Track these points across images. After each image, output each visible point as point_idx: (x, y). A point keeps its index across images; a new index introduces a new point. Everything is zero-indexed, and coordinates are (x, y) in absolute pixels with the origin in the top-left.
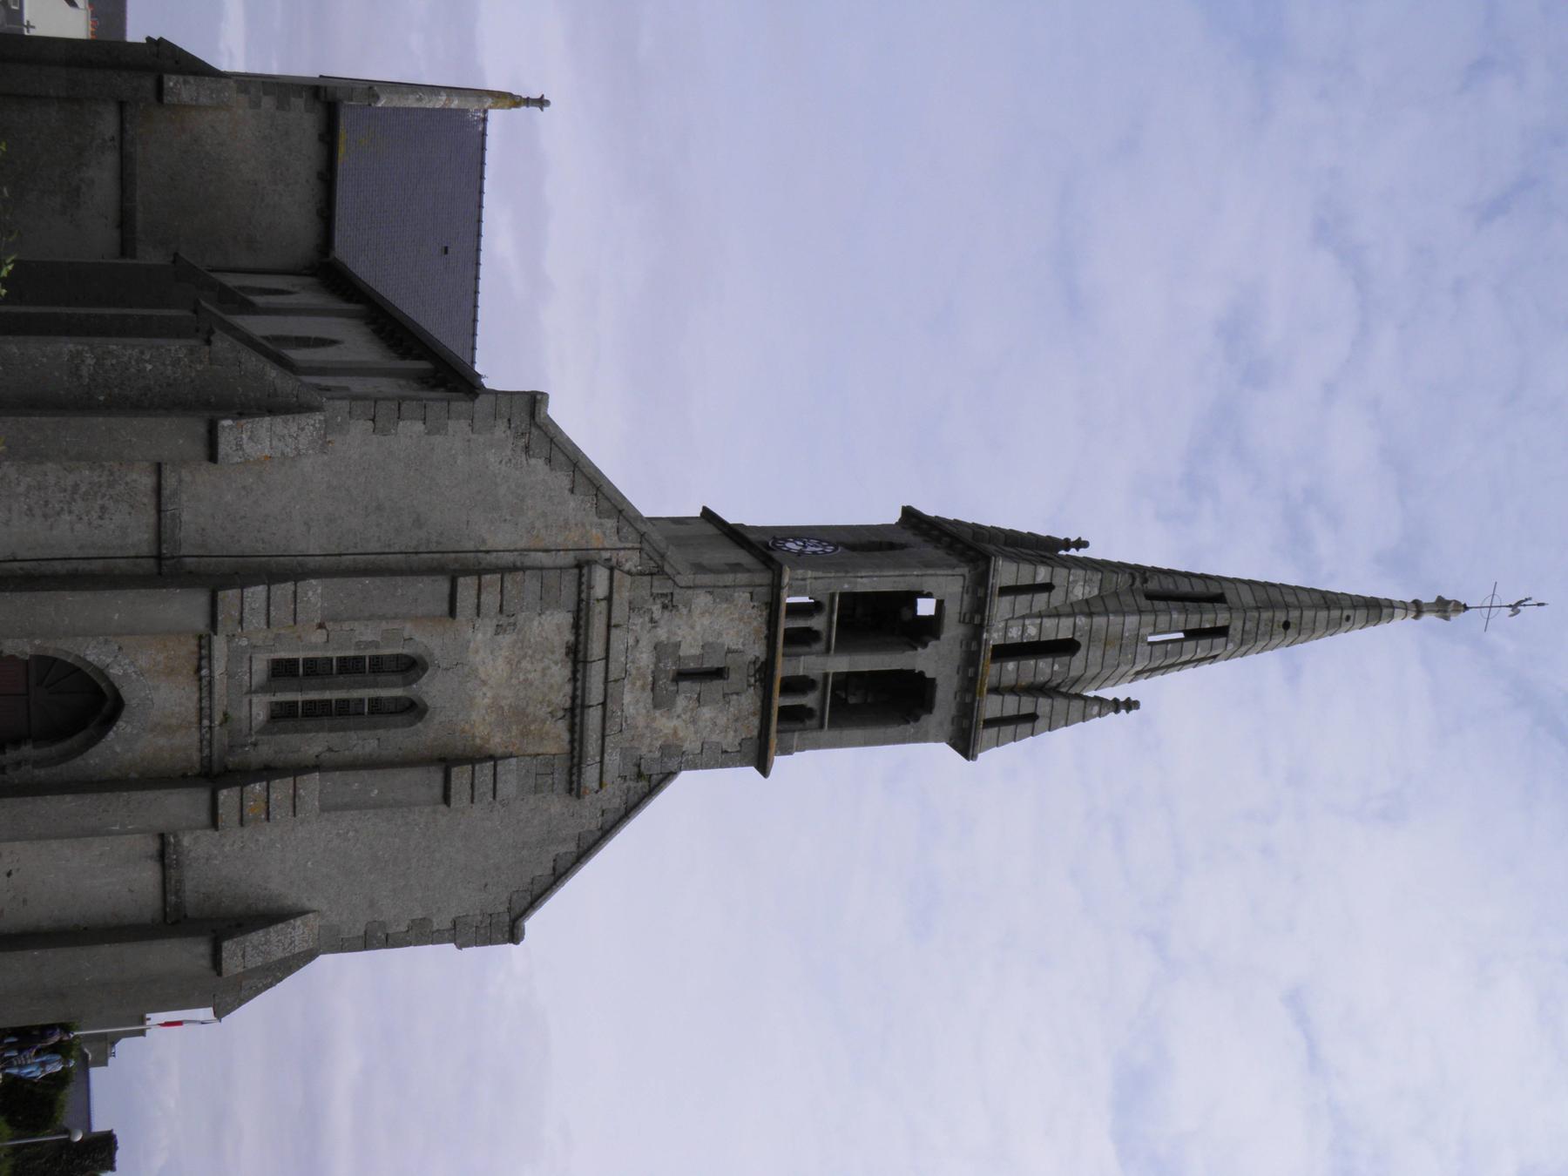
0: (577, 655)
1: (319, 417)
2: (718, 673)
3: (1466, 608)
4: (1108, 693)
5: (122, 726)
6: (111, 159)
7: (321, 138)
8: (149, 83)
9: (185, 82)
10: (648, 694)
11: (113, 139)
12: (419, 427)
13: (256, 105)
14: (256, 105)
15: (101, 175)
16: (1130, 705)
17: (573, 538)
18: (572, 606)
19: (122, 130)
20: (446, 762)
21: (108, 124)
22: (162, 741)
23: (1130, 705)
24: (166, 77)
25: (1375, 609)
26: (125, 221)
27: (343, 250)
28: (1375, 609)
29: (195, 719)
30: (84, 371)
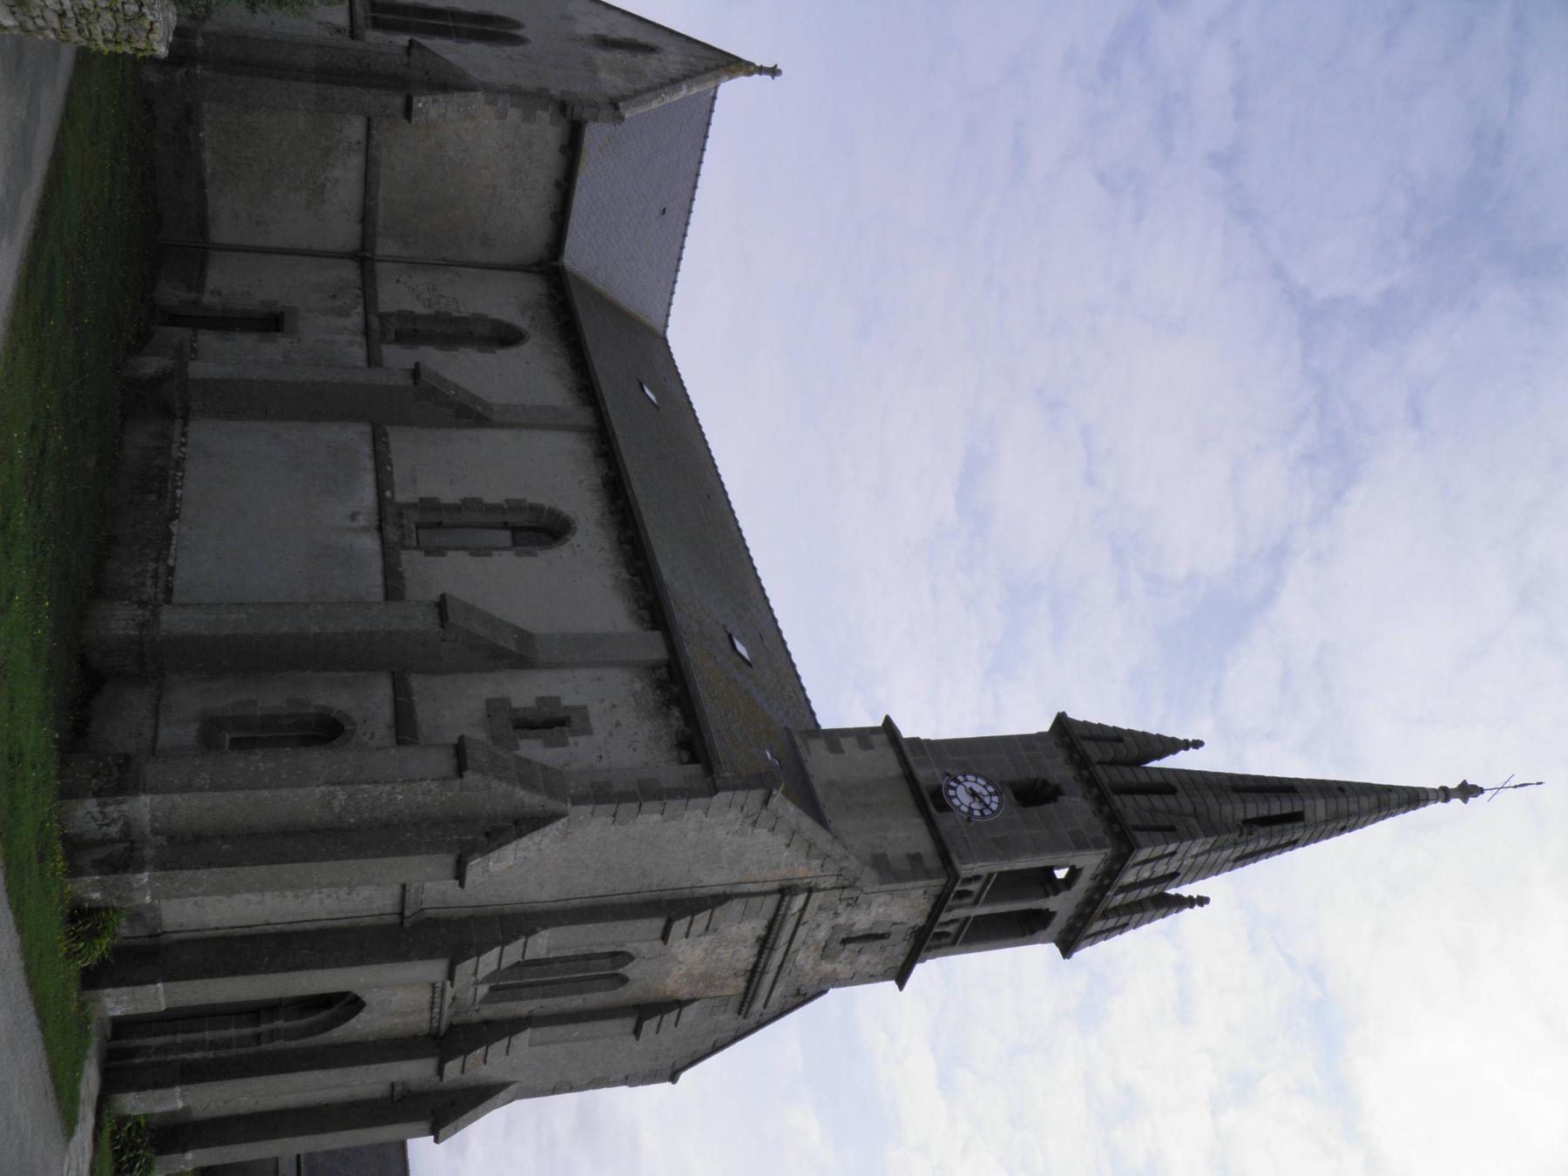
0: (765, 944)
1: (563, 820)
2: (882, 936)
3: (1481, 791)
4: (1186, 890)
5: (362, 1015)
6: (357, 160)
7: (563, 149)
8: (398, 101)
9: (434, 101)
10: (819, 952)
11: (359, 143)
12: (657, 817)
13: (502, 116)
14: (502, 116)
15: (346, 176)
16: (1202, 901)
17: (783, 872)
18: (769, 916)
19: (369, 136)
20: (646, 1011)
21: (355, 129)
22: (397, 1020)
23: (1202, 901)
24: (415, 99)
25: (1412, 798)
26: (366, 218)
27: (578, 257)
28: (1412, 798)
29: (427, 1007)
30: (336, 804)
